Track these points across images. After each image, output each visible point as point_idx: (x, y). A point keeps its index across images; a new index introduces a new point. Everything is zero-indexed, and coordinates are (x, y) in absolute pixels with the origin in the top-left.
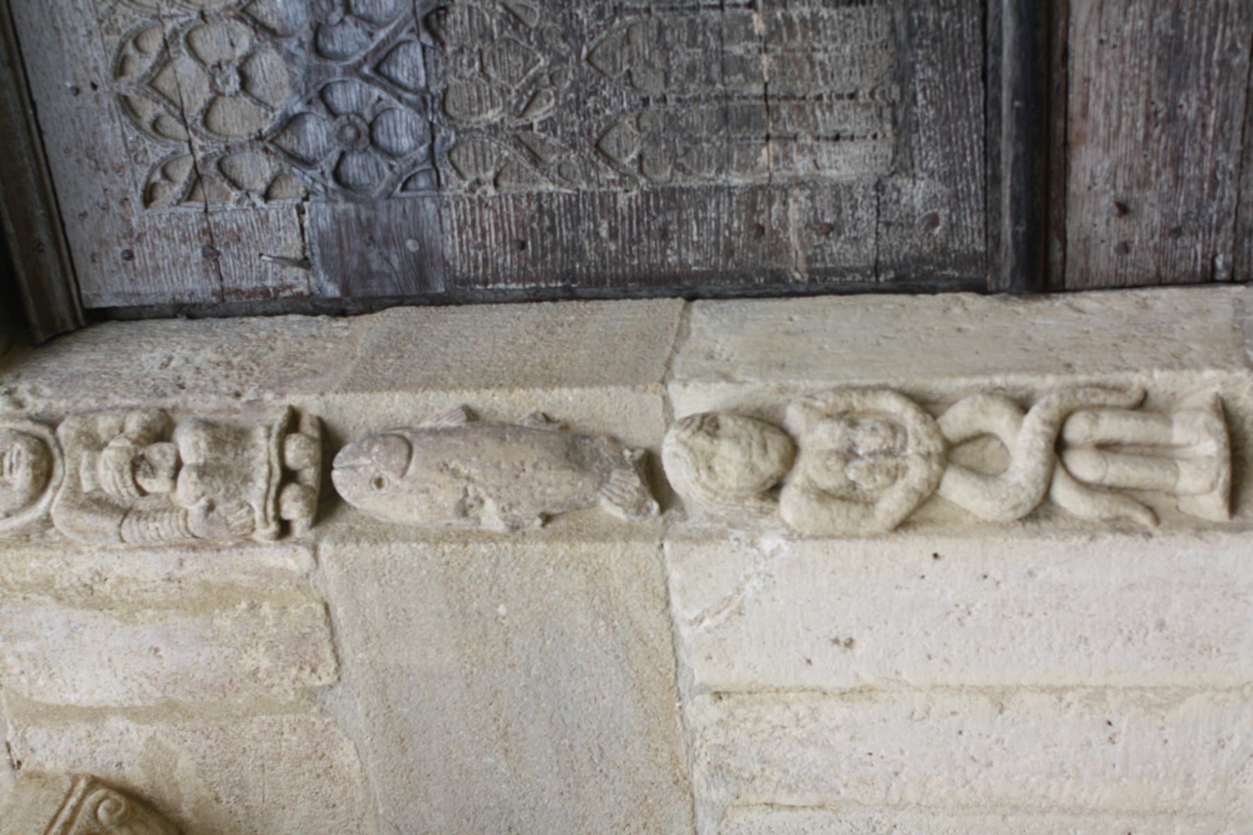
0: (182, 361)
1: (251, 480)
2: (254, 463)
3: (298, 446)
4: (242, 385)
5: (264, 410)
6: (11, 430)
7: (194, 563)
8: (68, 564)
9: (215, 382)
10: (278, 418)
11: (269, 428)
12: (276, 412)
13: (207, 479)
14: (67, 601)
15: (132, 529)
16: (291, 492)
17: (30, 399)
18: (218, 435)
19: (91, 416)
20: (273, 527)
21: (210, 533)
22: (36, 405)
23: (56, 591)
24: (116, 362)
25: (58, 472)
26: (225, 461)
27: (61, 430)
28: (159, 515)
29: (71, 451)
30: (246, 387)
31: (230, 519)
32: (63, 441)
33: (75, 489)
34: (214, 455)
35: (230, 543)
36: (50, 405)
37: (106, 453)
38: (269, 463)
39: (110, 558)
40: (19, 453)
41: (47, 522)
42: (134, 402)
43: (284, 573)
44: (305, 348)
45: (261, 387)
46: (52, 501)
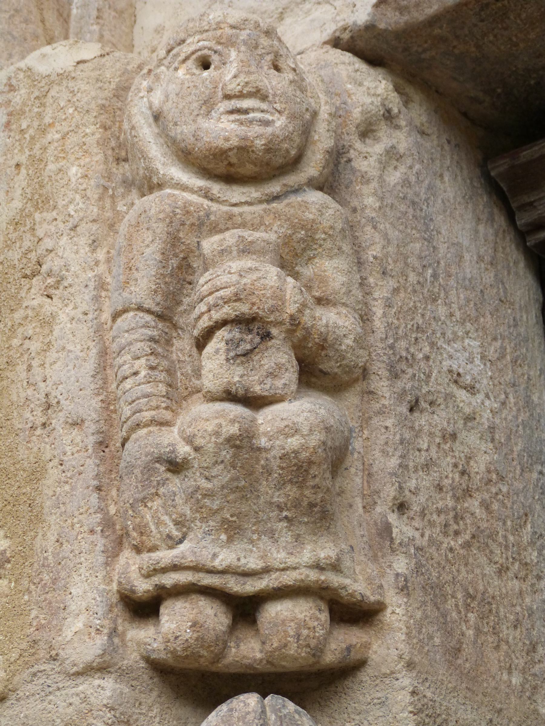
0: (467, 410)
1: (230, 540)
2: (265, 542)
3: (302, 624)
4: (423, 514)
5: (375, 558)
6: (315, 114)
7: (73, 447)
8: (74, 228)
9: (427, 466)
10: (356, 584)
11: (336, 567)
12: (369, 580)
13: (227, 454)
14: (13, 236)
15: (134, 330)
16: (213, 616)
17: (378, 149)
18: (314, 471)
19: (346, 248)
20: (143, 587)
21: (131, 467)
22: (366, 158)
23: (30, 215)
24: (458, 296)
25: (236, 194)
26: (264, 487)
27: (315, 197)
28: (162, 376)
29: (277, 215)
30: (417, 523)
31: (156, 504)
32: (294, 199)
33: (205, 225)
34: (275, 464)
35: (112, 510)
36: (366, 180)
37: (272, 274)
38: (267, 570)
39: (84, 300)
40: (267, 123)
41: (150, 184)
42: (378, 323)
43: (57, 611)
44: (505, 631)
45: (419, 549)
46: (184, 188)
